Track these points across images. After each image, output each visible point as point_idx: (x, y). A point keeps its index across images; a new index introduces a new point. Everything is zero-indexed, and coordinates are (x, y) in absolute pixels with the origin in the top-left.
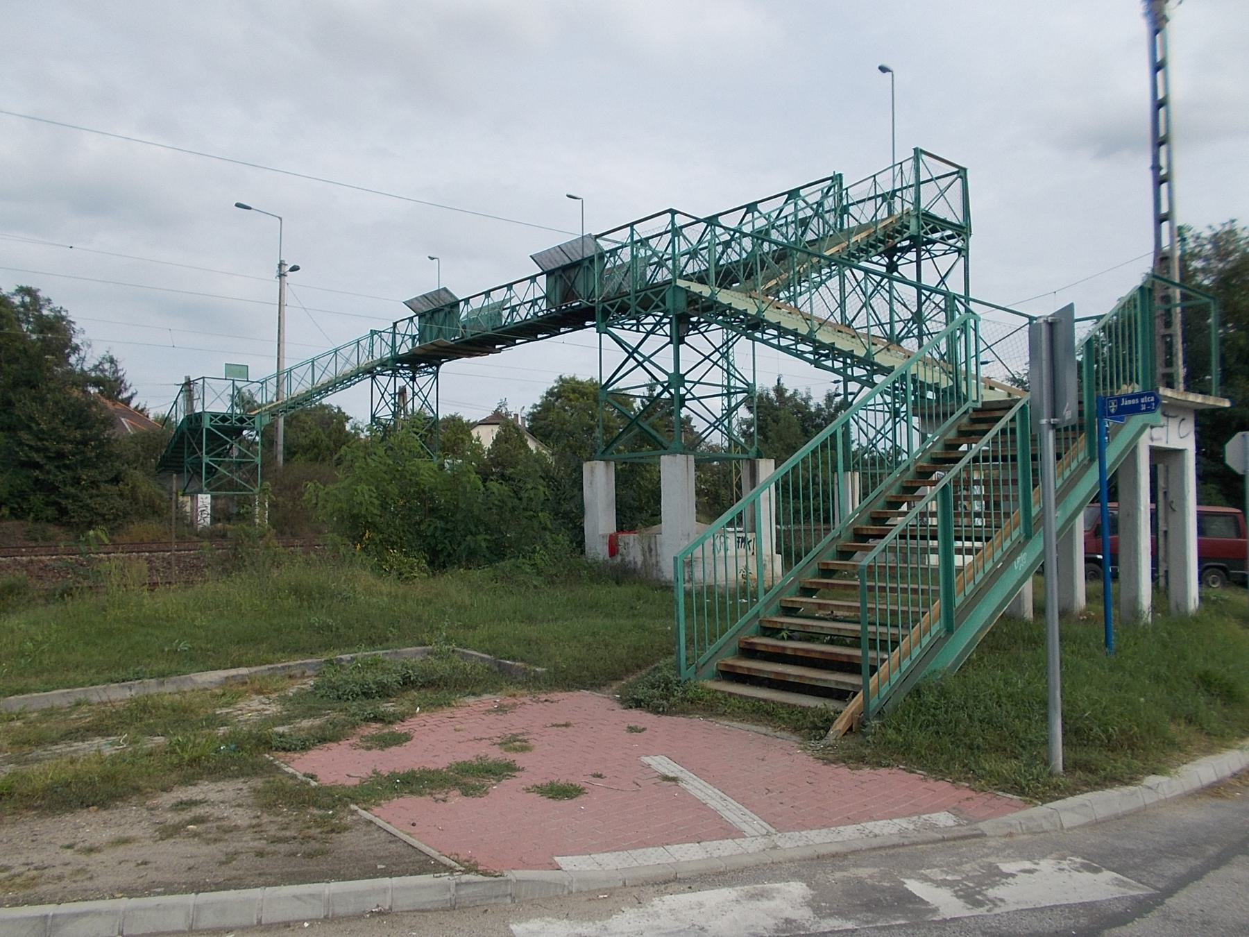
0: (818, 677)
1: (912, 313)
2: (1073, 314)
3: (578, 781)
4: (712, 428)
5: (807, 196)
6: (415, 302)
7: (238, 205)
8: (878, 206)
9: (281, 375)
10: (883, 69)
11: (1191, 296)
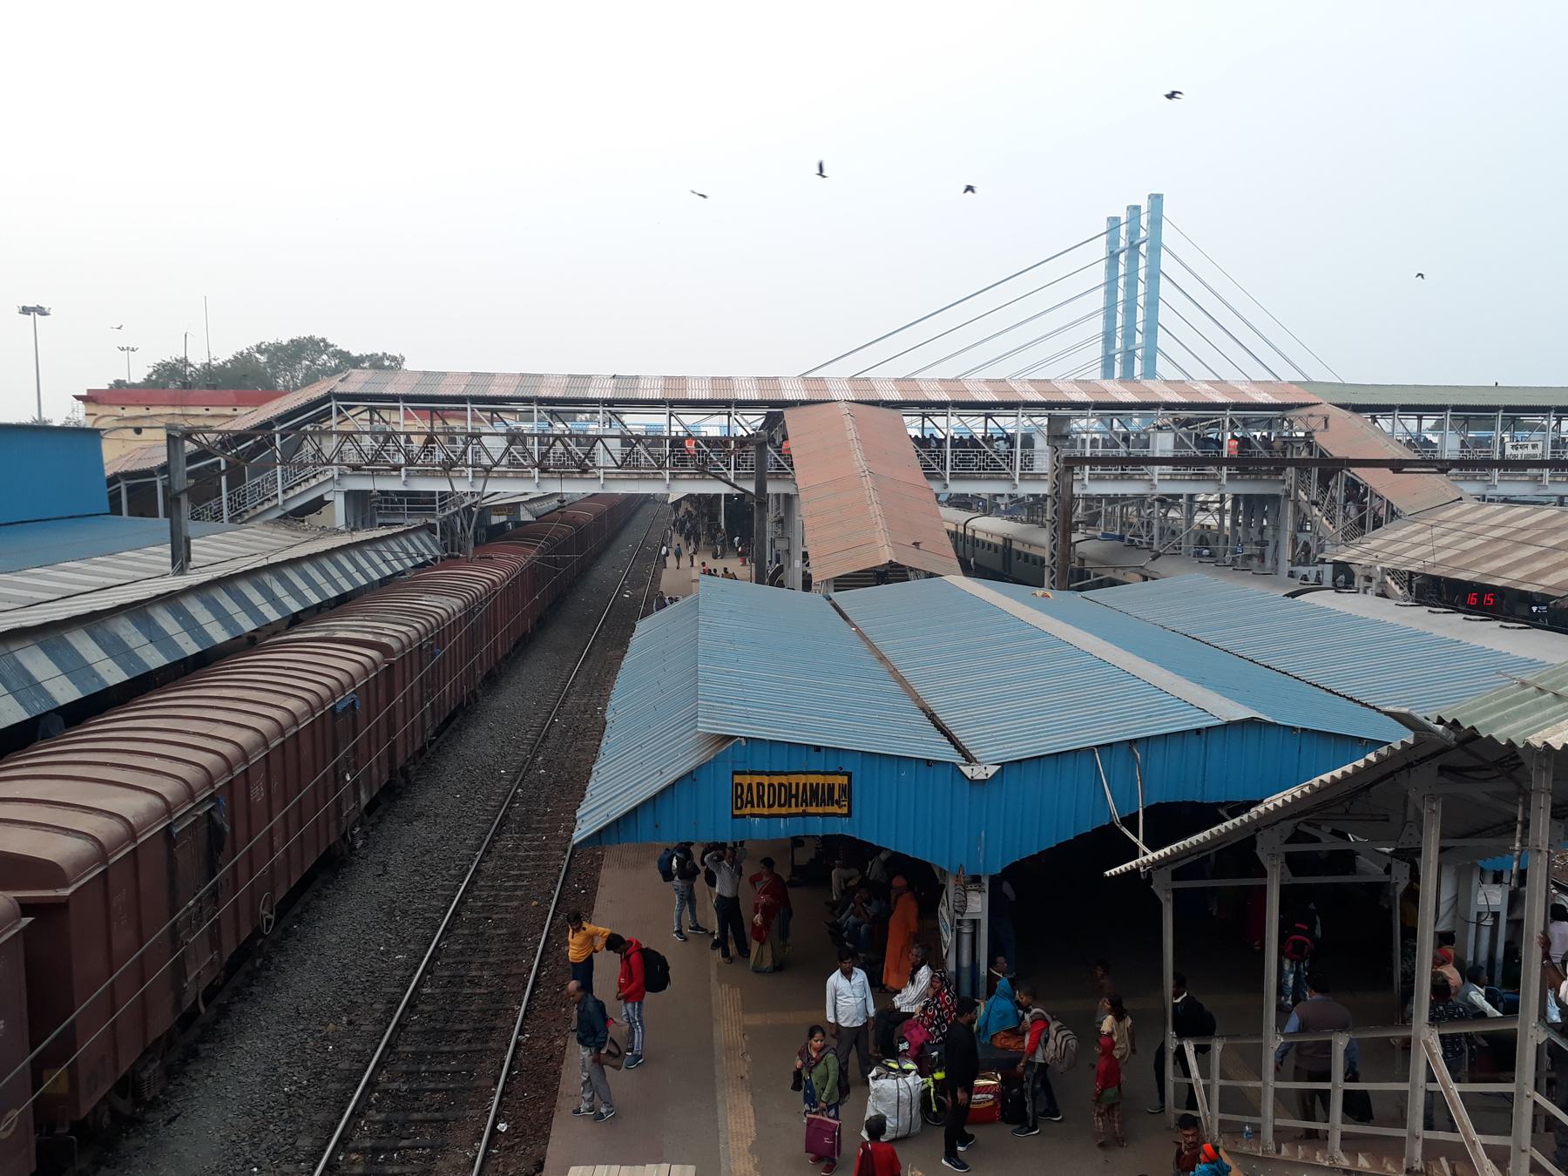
3: (693, 841)
4: (712, 765)
11: (32, 1052)
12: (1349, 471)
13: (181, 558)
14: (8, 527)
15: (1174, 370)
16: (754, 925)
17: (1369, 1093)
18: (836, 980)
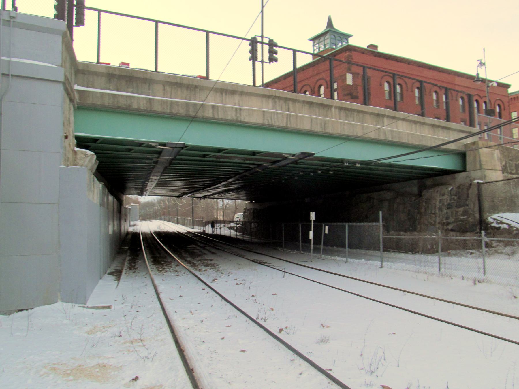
0: (150, 148)
1: (311, 128)
5: (245, 37)
6: (317, 114)
8: (415, 81)
9: (124, 231)
12: (338, 47)
13: (75, 6)
14: (247, 260)
15: (259, 17)
18: (311, 213)
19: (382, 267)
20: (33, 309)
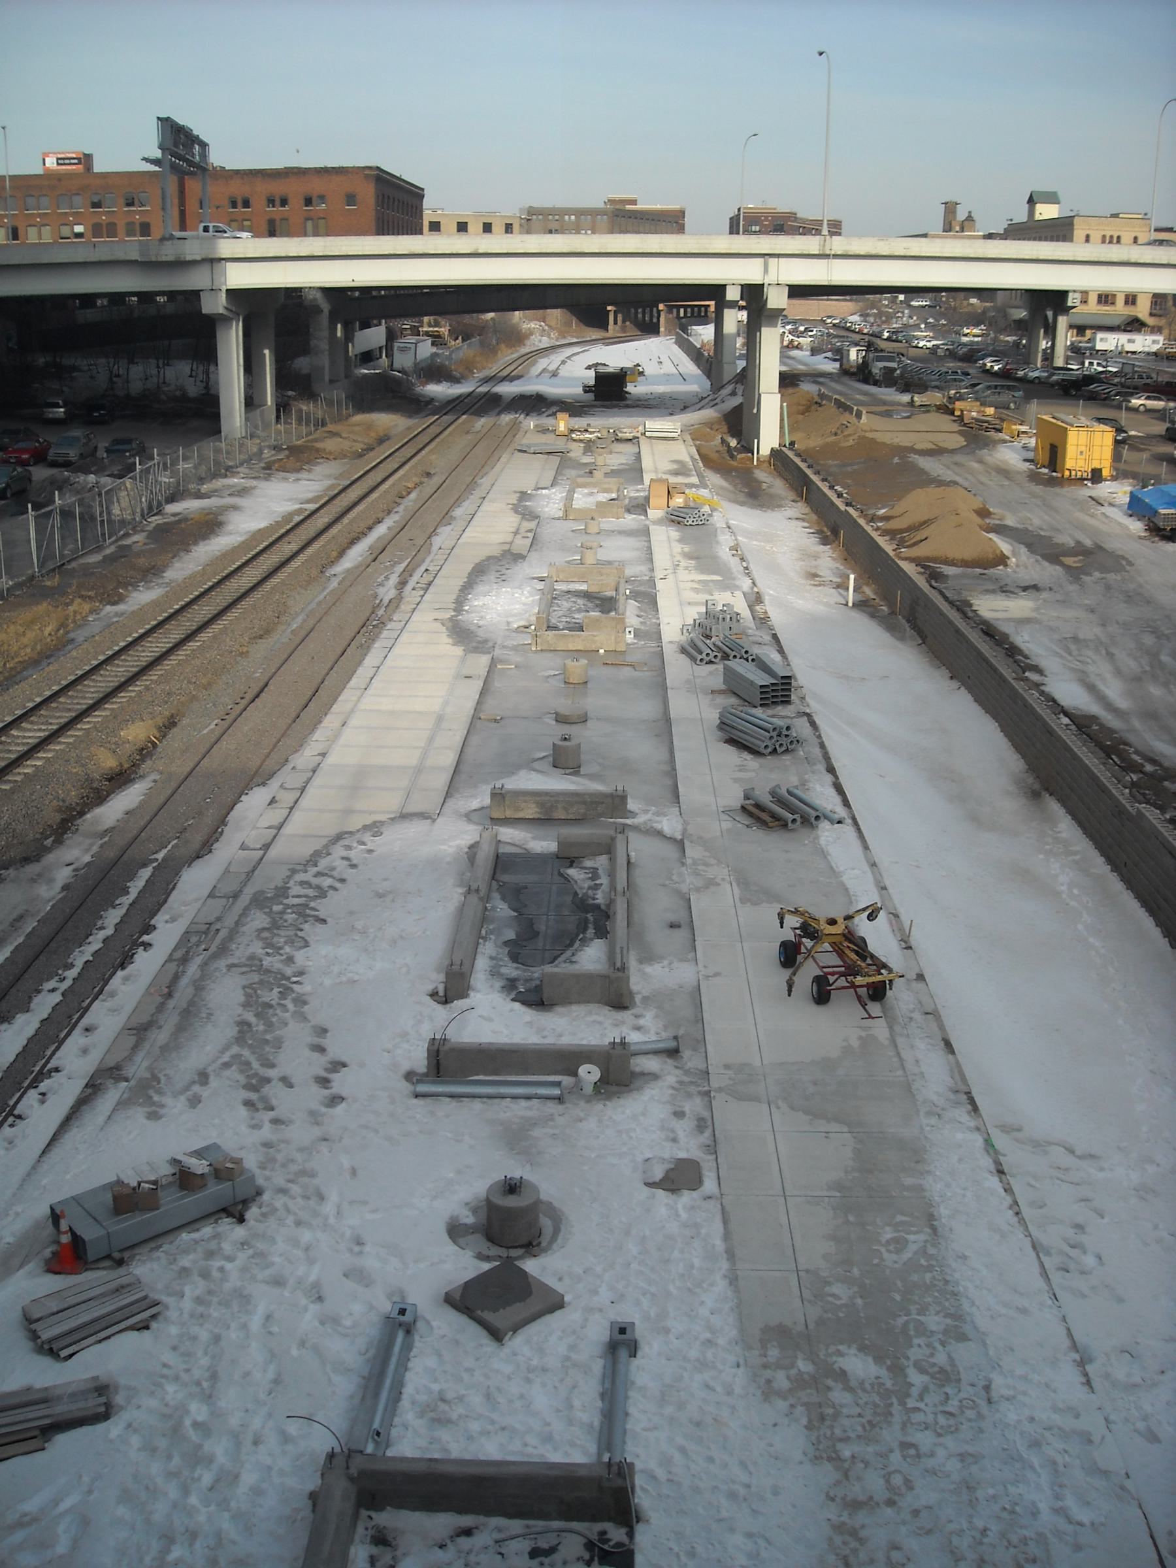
2: (765, 326)
7: (789, 995)
10: (821, 54)
16: (880, 301)
17: (178, 227)
19: (970, 212)
20: (534, 578)
